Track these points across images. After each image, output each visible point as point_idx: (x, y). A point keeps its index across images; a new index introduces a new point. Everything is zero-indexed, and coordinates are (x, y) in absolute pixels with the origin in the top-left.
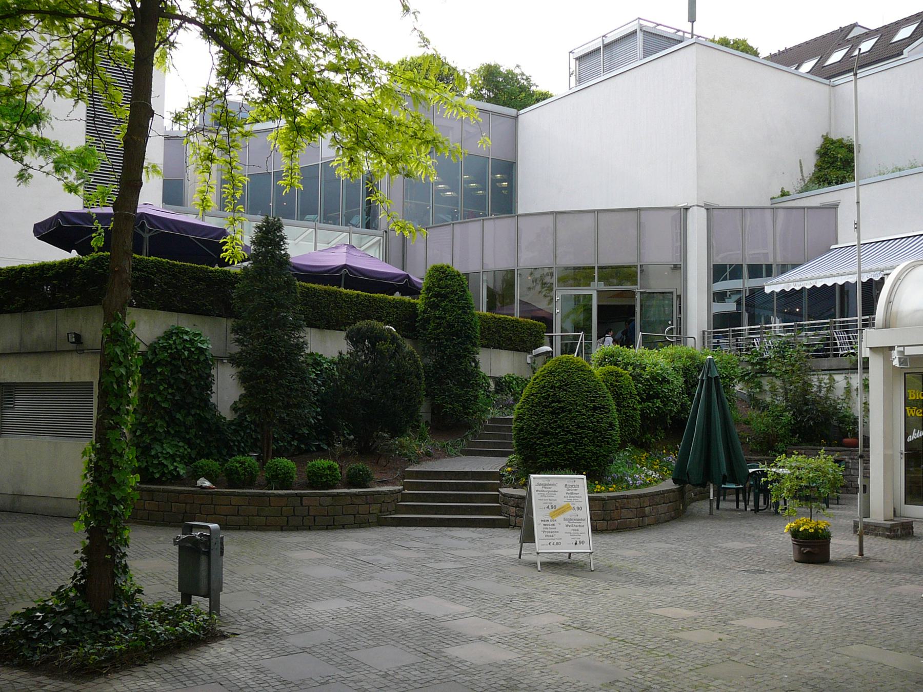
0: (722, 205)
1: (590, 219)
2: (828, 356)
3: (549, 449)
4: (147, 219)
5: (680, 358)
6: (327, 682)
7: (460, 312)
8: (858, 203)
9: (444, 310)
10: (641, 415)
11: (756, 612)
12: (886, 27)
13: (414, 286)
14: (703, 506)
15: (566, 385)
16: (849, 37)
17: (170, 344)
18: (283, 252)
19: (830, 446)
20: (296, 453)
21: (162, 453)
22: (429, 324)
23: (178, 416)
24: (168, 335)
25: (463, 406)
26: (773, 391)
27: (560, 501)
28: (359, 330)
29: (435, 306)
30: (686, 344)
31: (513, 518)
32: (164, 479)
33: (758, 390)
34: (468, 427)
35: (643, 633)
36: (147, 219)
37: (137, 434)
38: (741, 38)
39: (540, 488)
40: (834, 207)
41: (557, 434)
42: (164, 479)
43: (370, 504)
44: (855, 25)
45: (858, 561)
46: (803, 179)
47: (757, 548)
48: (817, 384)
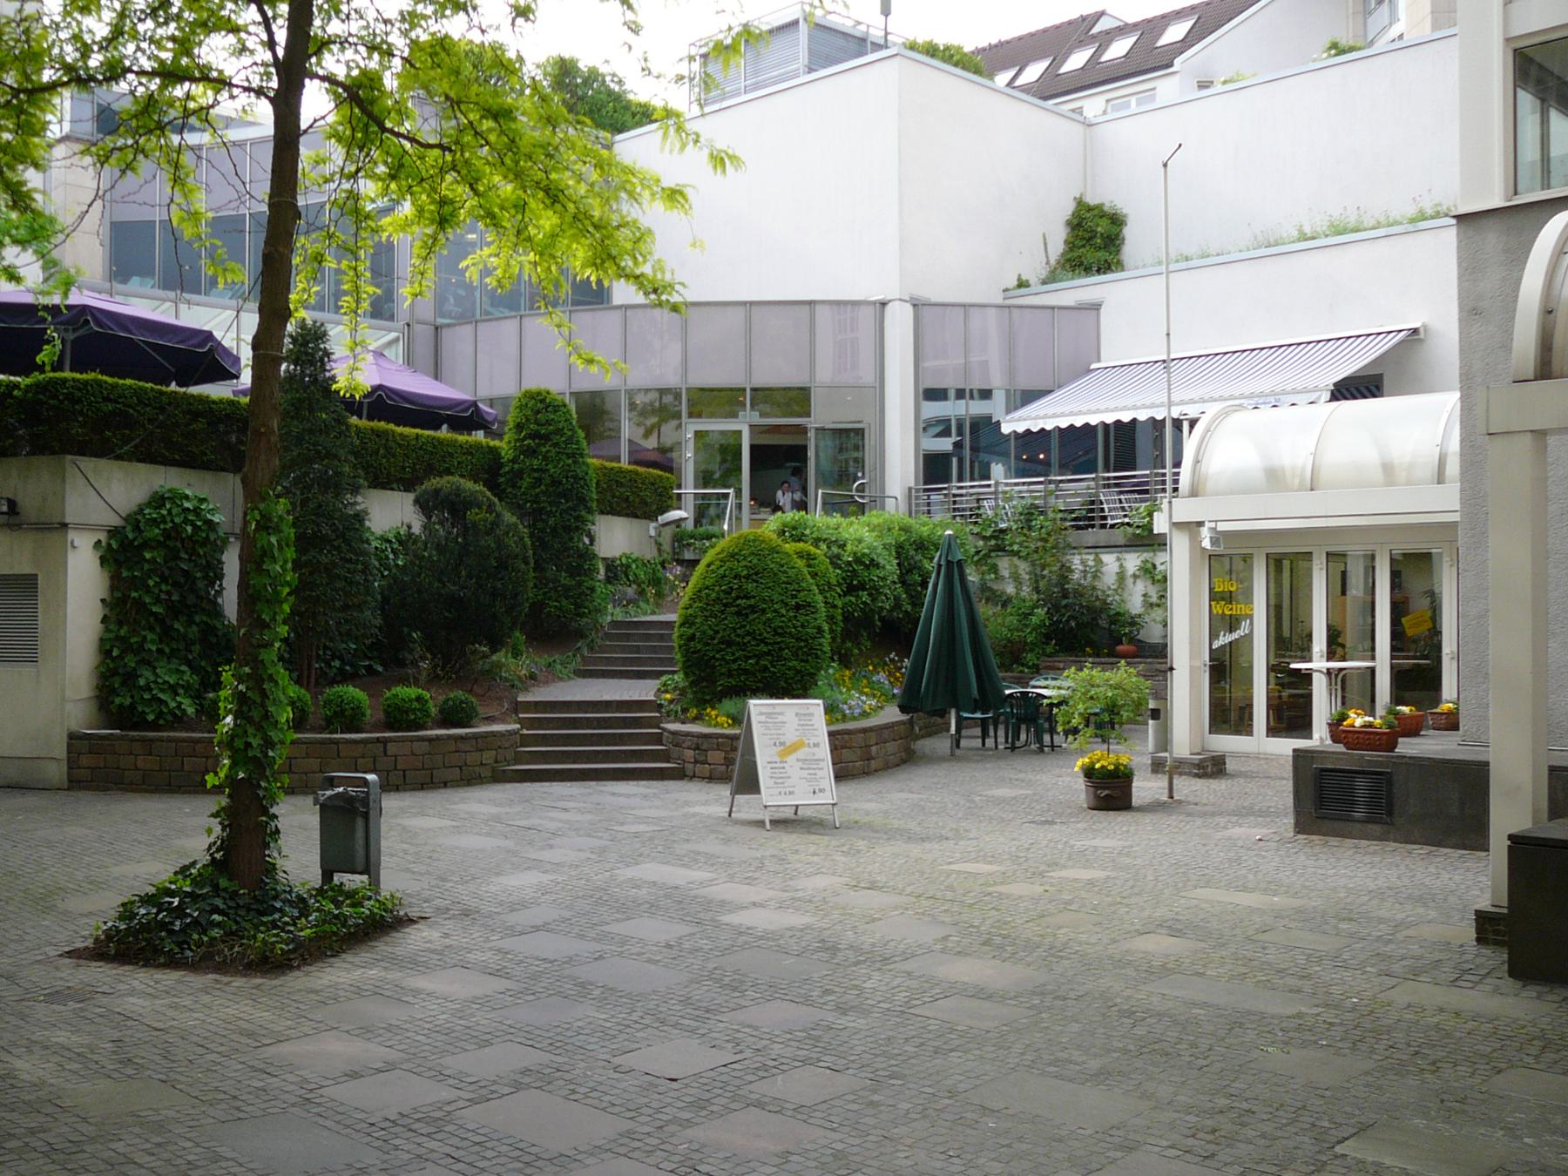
0: (934, 299)
1: (739, 314)
2: (1093, 526)
3: (735, 666)
4: (93, 315)
5: (889, 530)
6: (601, 957)
7: (570, 461)
8: (1168, 334)
9: (545, 458)
10: (843, 614)
11: (1070, 863)
12: (1149, 21)
13: (483, 418)
14: (942, 744)
15: (756, 574)
16: (1095, 31)
17: (163, 516)
18: (327, 374)
19: (1098, 656)
20: (339, 679)
21: (155, 682)
22: (521, 479)
23: (177, 626)
24: (158, 500)
25: (575, 604)
26: (1016, 578)
27: (790, 736)
28: (437, 491)
29: (531, 452)
30: (883, 508)
31: (690, 766)
32: (161, 722)
33: (993, 576)
34: (580, 634)
35: (951, 888)
36: (93, 315)
37: (114, 654)
38: (956, 43)
39: (763, 718)
40: (1096, 307)
41: (745, 644)
42: (161, 722)
43: (481, 750)
44: (1102, 13)
45: (1168, 805)
46: (1048, 263)
47: (1035, 794)
48: (1081, 568)
